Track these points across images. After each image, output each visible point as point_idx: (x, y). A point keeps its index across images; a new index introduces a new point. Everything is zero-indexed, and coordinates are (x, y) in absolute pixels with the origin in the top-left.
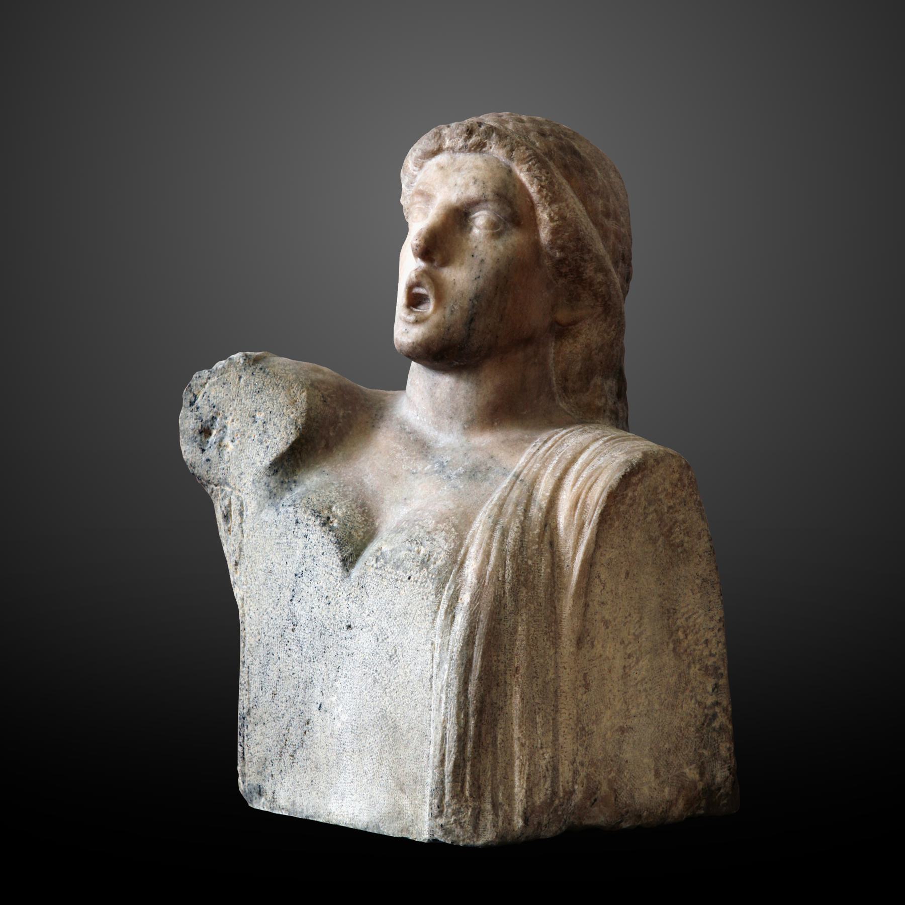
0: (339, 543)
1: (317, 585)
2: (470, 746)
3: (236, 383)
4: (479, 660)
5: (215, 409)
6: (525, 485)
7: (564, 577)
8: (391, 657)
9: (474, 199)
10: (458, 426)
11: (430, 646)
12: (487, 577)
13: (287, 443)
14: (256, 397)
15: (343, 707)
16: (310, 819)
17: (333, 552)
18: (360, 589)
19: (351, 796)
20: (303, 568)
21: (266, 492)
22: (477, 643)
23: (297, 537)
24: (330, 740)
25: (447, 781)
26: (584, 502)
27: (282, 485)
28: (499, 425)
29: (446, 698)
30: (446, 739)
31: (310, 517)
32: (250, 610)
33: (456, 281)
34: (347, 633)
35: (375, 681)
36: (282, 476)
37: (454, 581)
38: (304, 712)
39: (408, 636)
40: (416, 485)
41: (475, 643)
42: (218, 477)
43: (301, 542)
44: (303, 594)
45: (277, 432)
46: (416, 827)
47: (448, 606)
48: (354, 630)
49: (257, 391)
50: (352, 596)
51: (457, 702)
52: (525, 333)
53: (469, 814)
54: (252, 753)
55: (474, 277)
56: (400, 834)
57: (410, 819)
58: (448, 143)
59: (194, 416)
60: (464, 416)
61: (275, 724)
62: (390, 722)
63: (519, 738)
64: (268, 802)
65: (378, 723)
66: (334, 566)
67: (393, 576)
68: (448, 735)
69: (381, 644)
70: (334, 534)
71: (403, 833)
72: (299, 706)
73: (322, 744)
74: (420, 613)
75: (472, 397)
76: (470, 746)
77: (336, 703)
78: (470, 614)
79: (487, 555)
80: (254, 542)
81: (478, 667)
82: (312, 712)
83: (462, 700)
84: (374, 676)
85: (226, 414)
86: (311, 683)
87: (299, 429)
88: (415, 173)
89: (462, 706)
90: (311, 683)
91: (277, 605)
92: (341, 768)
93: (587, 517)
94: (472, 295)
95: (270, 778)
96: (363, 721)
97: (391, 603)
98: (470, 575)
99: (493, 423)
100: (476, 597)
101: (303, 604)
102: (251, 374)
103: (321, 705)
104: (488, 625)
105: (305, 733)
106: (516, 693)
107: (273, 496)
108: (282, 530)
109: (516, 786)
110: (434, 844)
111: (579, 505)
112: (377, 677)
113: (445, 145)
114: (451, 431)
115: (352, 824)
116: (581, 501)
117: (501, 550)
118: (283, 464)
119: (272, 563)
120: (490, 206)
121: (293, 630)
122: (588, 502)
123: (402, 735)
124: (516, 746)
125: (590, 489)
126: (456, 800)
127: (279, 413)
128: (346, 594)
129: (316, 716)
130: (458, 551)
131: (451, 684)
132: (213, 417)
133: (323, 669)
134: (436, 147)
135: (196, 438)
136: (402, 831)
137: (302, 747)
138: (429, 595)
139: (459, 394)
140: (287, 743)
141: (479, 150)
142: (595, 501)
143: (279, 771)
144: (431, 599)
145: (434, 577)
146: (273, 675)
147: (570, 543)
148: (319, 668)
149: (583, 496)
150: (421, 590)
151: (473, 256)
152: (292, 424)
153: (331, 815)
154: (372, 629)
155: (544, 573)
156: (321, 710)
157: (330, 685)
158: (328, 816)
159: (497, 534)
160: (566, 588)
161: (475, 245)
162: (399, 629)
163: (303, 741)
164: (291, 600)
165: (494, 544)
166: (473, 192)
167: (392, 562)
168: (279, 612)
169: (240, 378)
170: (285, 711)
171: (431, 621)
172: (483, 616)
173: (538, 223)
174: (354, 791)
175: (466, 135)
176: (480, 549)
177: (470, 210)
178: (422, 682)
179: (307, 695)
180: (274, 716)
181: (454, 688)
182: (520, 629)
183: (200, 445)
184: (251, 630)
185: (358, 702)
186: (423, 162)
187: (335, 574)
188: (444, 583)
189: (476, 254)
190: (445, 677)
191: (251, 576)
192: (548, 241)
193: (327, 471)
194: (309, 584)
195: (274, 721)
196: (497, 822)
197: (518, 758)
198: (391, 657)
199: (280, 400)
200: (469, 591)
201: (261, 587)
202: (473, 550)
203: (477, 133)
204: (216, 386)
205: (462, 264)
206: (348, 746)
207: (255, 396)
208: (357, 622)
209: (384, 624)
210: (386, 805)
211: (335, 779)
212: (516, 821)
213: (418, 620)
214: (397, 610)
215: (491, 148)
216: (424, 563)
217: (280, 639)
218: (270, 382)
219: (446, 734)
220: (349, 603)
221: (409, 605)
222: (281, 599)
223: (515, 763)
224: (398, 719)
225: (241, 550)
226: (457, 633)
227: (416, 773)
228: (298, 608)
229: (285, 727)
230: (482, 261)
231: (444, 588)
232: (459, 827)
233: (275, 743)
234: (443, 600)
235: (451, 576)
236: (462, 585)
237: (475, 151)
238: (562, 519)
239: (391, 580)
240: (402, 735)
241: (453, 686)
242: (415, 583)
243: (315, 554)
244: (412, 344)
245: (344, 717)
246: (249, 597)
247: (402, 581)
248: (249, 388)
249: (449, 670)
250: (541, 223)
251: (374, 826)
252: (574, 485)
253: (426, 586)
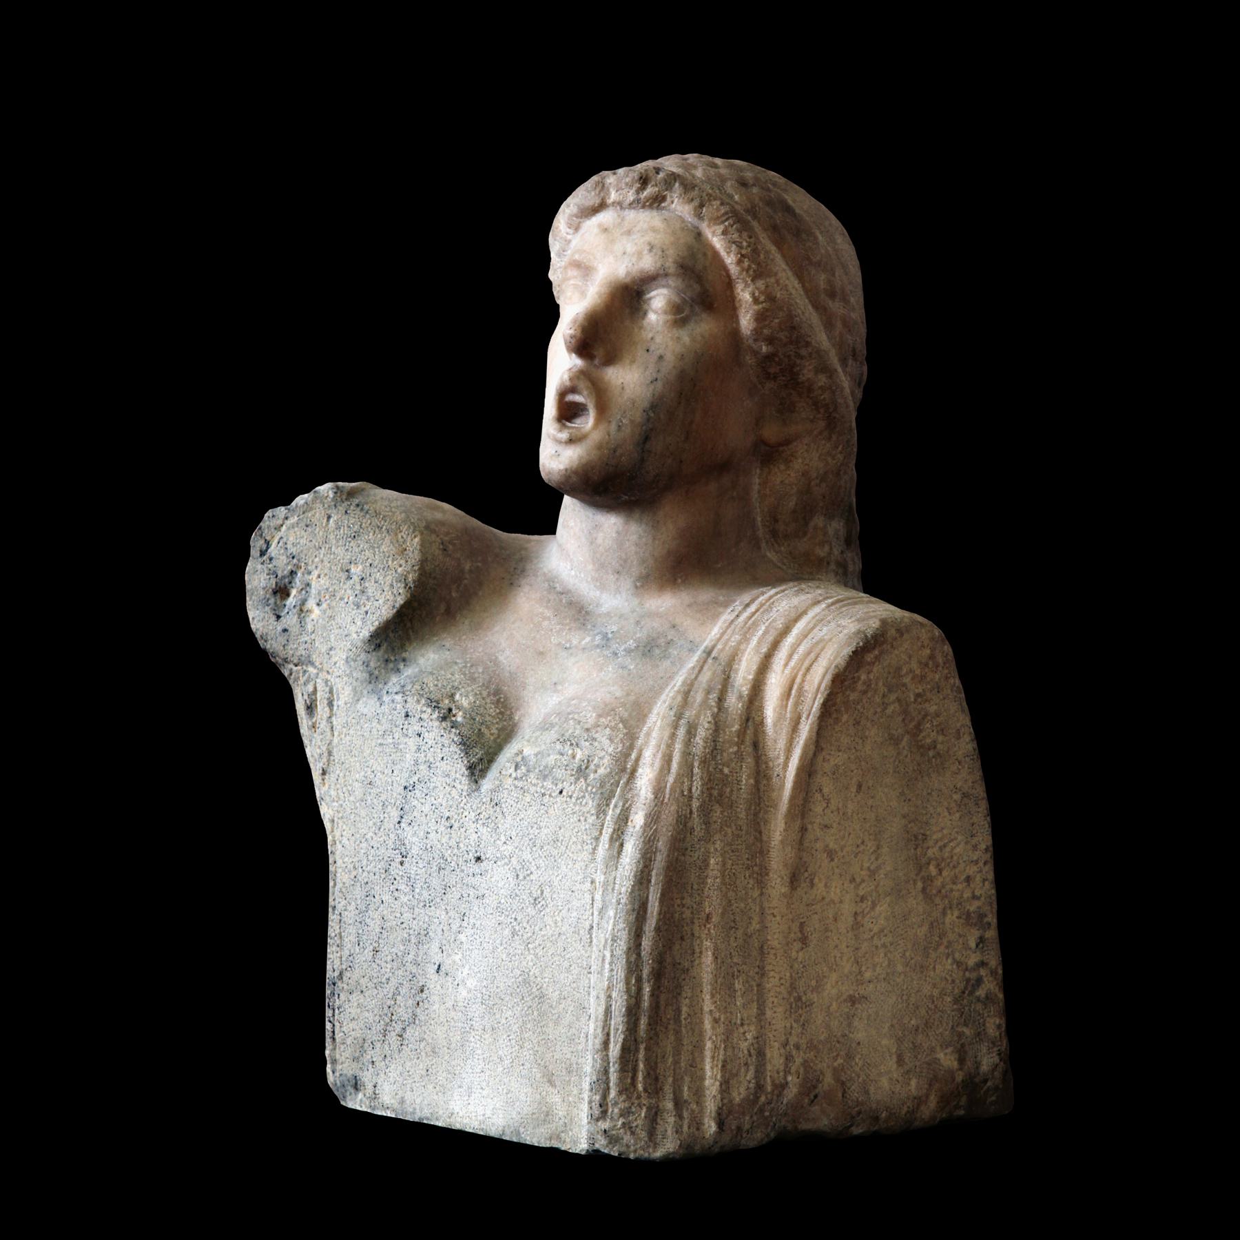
0: (464, 744)
1: (435, 802)
2: (643, 1022)
3: (324, 525)
4: (657, 904)
5: (295, 561)
6: (720, 664)
7: (773, 790)
8: (535, 900)
9: (650, 273)
10: (627, 583)
11: (589, 885)
12: (668, 791)
13: (394, 607)
14: (351, 544)
15: (470, 969)
16: (425, 1122)
17: (456, 757)
18: (493, 807)
19: (481, 1091)
20: (415, 779)
21: (364, 674)
22: (653, 881)
23: (407, 735)
24: (453, 1014)
25: (612, 1070)
26: (801, 689)
27: (386, 664)
28: (683, 582)
29: (611, 956)
30: (611, 1012)
31: (425, 709)
32: (342, 836)
33: (624, 385)
34: (476, 868)
35: (514, 933)
36: (386, 652)
37: (623, 796)
38: (417, 975)
39: (560, 872)
40: (570, 664)
41: (650, 881)
42: (299, 653)
43: (412, 743)
44: (415, 814)
45: (380, 592)
46: (570, 1133)
47: (614, 830)
48: (485, 863)
49: (353, 535)
50: (482, 816)
51: (626, 962)
53: (643, 1115)
54: (346, 1032)
55: (650, 379)
56: (548, 1142)
57: (561, 1122)
58: (613, 196)
59: (265, 569)
60: (636, 570)
61: (376, 992)
62: (534, 990)
63: (711, 1011)
64: (367, 1098)
65: (518, 990)
66: (458, 776)
67: (539, 789)
68: (613, 1007)
69: (522, 883)
70: (458, 731)
71: (552, 1142)
72: (410, 967)
73: (442, 1020)
74: (575, 839)
75: (646, 544)
76: (643, 1022)
77: (460, 963)
78: (643, 841)
79: (668, 760)
80: (348, 743)
81: (655, 913)
82: (428, 976)
83: (633, 959)
84: (513, 927)
85: (309, 568)
86: (426, 936)
87: (410, 588)
88: (569, 237)
89: (633, 968)
90: (426, 936)
91: (380, 829)
92: (468, 1053)
93: (805, 708)
94: (646, 404)
95: (370, 1066)
96: (497, 987)
97: (536, 826)
98: (644, 788)
99: (676, 580)
100: (653, 818)
101: (416, 828)
102: (344, 512)
103: (439, 966)
104: (668, 856)
105: (418, 1004)
106: (706, 949)
107: (374, 679)
108: (386, 726)
109: (707, 1077)
110: (594, 1157)
111: (793, 692)
112: (517, 928)
113: (609, 198)
114: (618, 591)
115: (482, 1129)
116: (795, 687)
117: (687, 754)
118: (387, 636)
119: (373, 772)
120: (671, 282)
121: (402, 863)
122: (806, 688)
123: (551, 1007)
124: (706, 1022)
125: (808, 670)
126: (624, 1096)
127: (382, 567)
128: (474, 814)
129: (433, 981)
130: (627, 755)
131: (617, 937)
132: (292, 571)
133: (443, 917)
134: (598, 201)
135: (268, 600)
136: (550, 1139)
137: (414, 1023)
138: (588, 815)
139: (628, 540)
140: (393, 1018)
141: (656, 205)
142: (816, 686)
143: (383, 1056)
144: (591, 821)
145: (594, 790)
146: (374, 926)
147: (782, 744)
148: (437, 916)
149: (798, 680)
150: (577, 808)
151: (648, 350)
152: (400, 581)
153: (454, 1116)
154: (510, 861)
155: (746, 785)
156: (440, 973)
157: (453, 939)
158: (450, 1118)
159: (681, 732)
160: (776, 805)
161: (650, 335)
162: (547, 862)
163: (415, 1015)
164: (399, 822)
165: (677, 746)
166: (648, 263)
167: (537, 771)
168: (382, 839)
169: (329, 517)
170: (391, 974)
171: (591, 851)
172: (662, 844)
173: (737, 305)
174: (484, 1084)
175: (638, 185)
176: (658, 752)
177: (644, 288)
178: (579, 934)
179: (421, 953)
180: (375, 981)
181: (622, 943)
182: (712, 861)
183: (274, 610)
184: (344, 863)
185: (491, 961)
186: (580, 222)
187: (459, 786)
188: (609, 799)
189: (652, 348)
190: (610, 928)
191: (344, 789)
192: (751, 331)
193: (448, 645)
194: (423, 801)
195: (376, 988)
196: (681, 1127)
197: (710, 1038)
198: (535, 900)
199: (384, 548)
200: (643, 810)
201: (358, 804)
202: (648, 754)
203: (653, 183)
204: (296, 529)
205: (633, 362)
206: (476, 1022)
207: (350, 542)
208: (489, 853)
209: (527, 856)
210: (528, 1103)
211: (459, 1068)
212: (707, 1125)
213: (572, 850)
214: (544, 836)
215: (672, 202)
216: (581, 772)
217: (383, 876)
218: (370, 524)
219: (611, 1006)
220: (478, 826)
221: (560, 829)
222: (386, 820)
223: (705, 1045)
224: (545, 985)
225: (330, 754)
226: (627, 867)
227: (570, 1060)
228: (408, 833)
229: (390, 996)
230: (661, 357)
231: (608, 805)
232: (629, 1133)
233: (377, 1018)
234: (607, 823)
235: (619, 789)
236: (633, 802)
237: (651, 207)
238: (770, 711)
239: (536, 795)
240: (551, 1007)
241: (621, 940)
242: (568, 799)
243: (432, 760)
244: (564, 472)
245: (471, 983)
246: (342, 818)
247: (550, 796)
248: (342, 531)
249: (615, 918)
250: (741, 306)
251: (512, 1132)
252: (786, 665)
253: (583, 803)
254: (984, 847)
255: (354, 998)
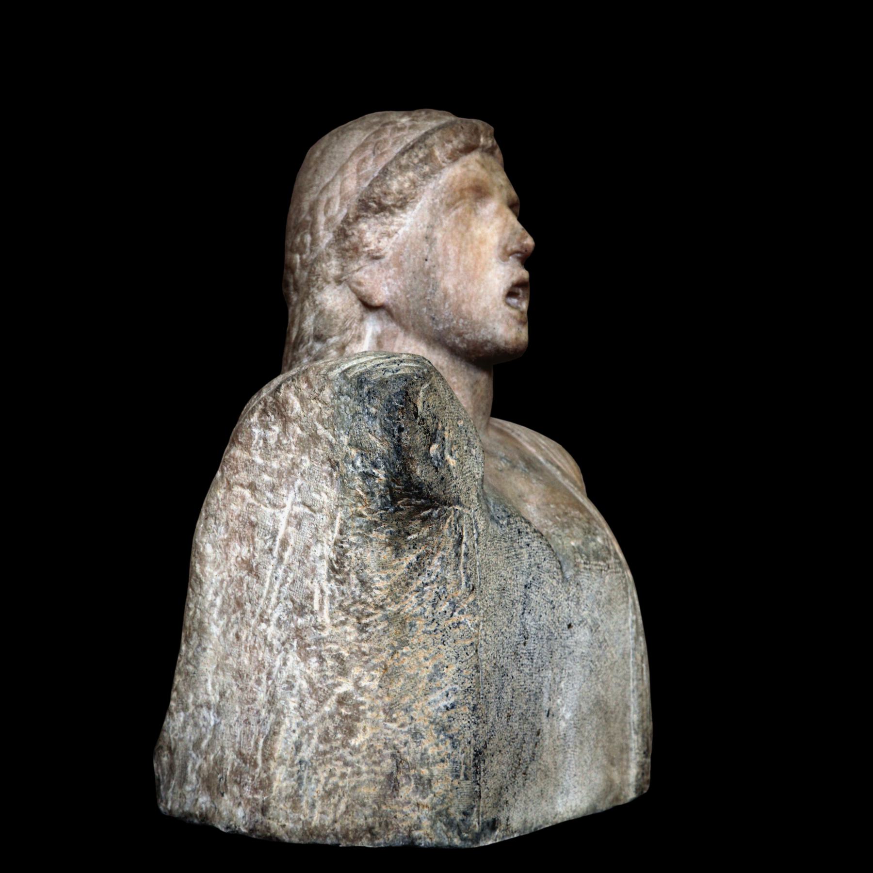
16: (539, 829)
35: (591, 671)
52: (466, 181)
88: (444, 164)
101: (533, 615)
121: (525, 644)
146: (507, 698)
164: (523, 613)
187: (557, 577)
208: (576, 620)
243: (538, 562)
254: (313, 677)
255: (495, 759)
